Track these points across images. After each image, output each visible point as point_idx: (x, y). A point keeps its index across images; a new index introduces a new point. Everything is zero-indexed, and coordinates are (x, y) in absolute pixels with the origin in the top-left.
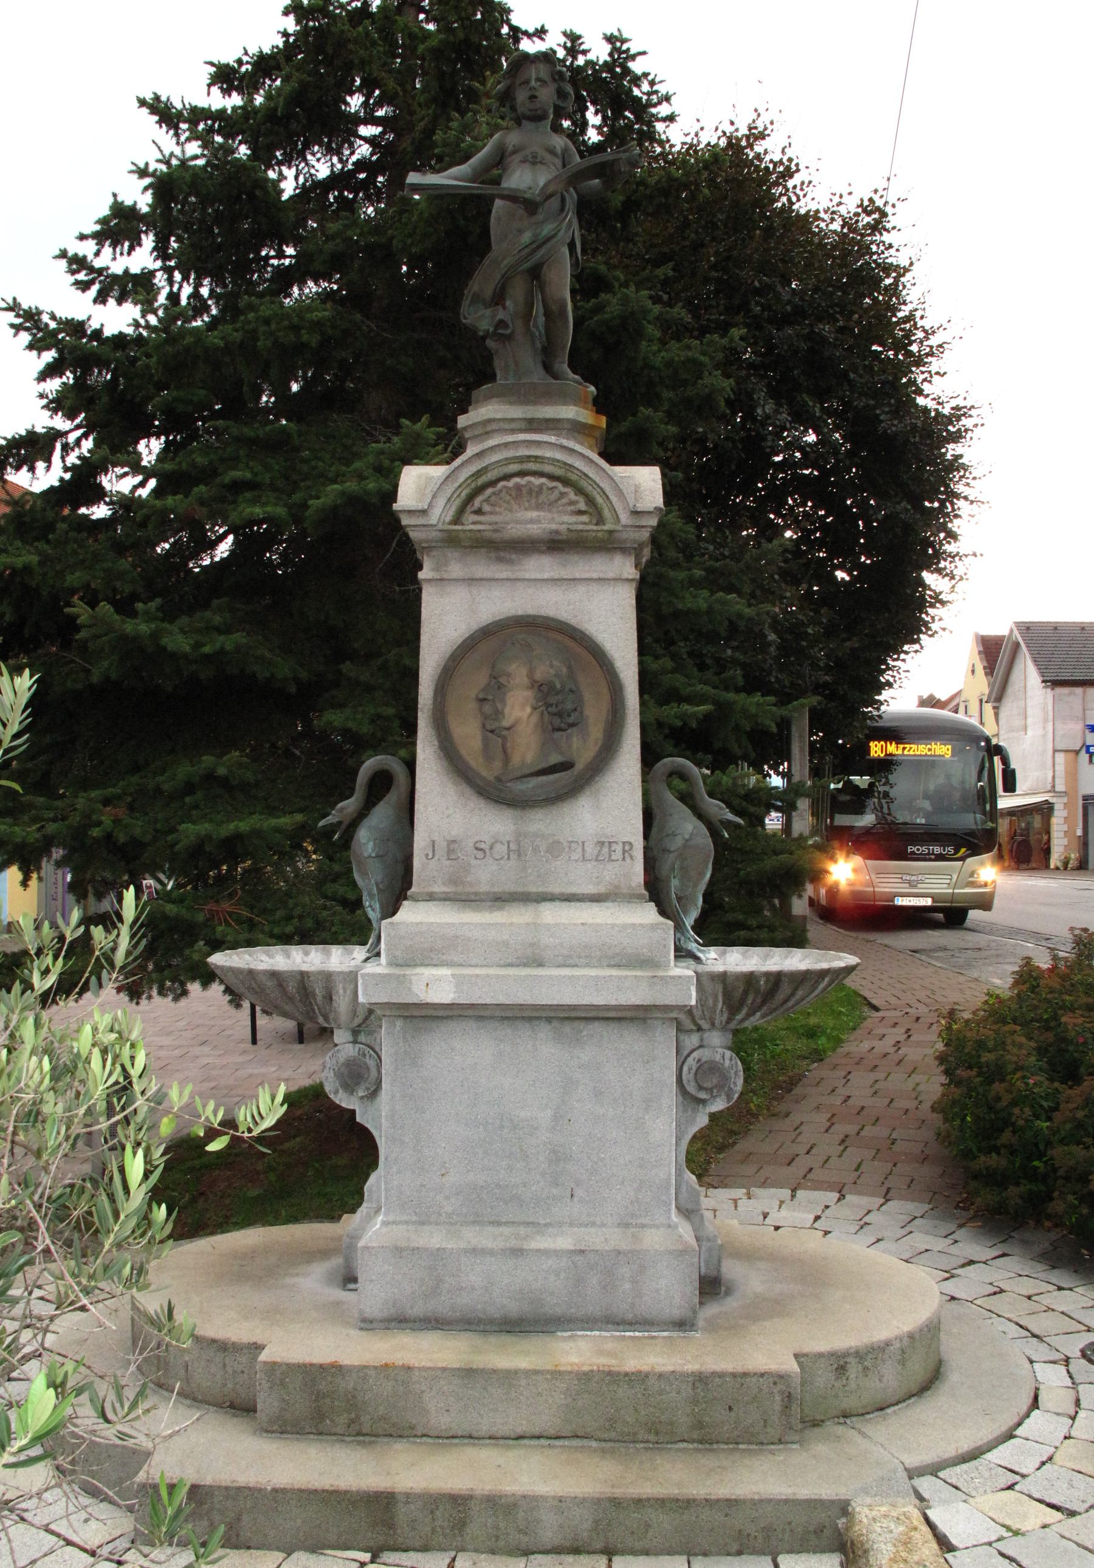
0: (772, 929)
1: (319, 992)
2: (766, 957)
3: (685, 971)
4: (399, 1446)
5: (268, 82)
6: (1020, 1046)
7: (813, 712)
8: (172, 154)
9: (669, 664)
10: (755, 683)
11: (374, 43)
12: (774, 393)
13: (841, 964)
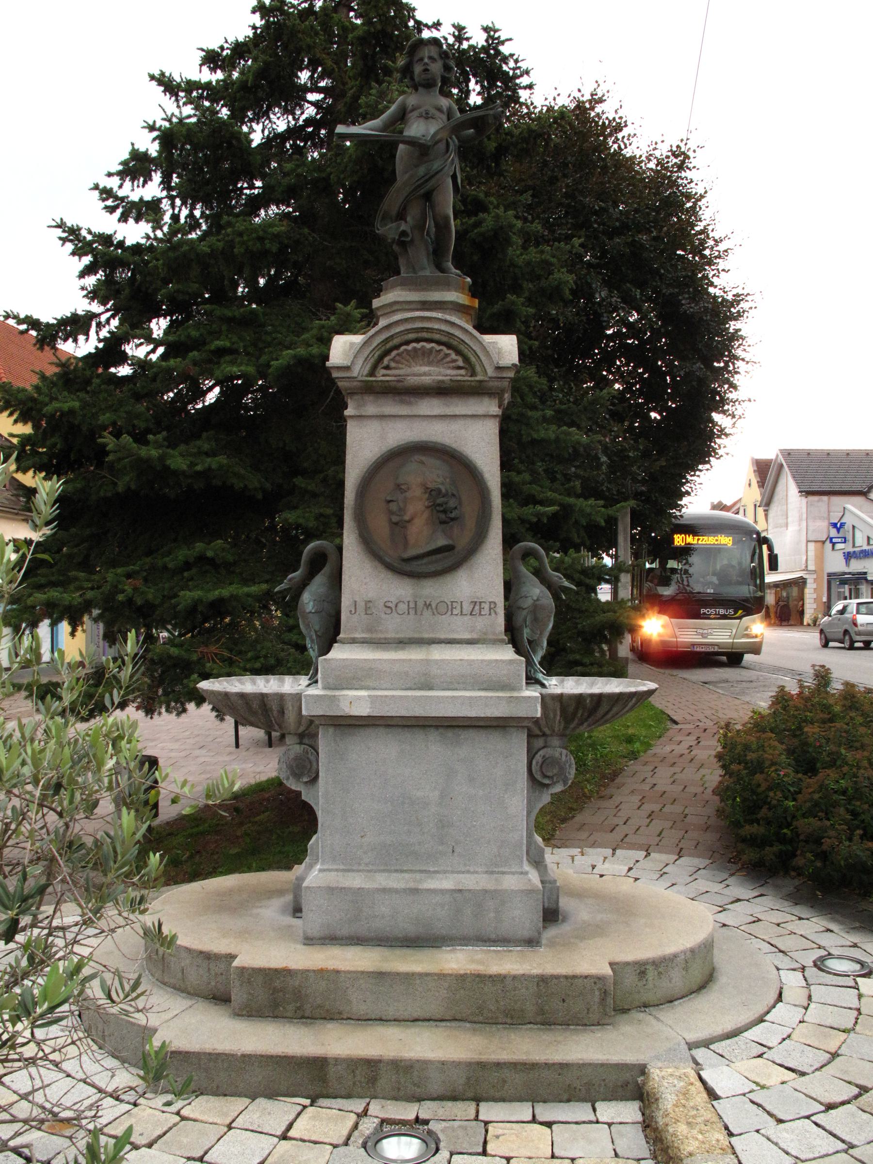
0: (600, 666)
1: (275, 708)
2: (592, 685)
3: (533, 692)
4: (330, 1025)
5: (242, 62)
6: (775, 748)
7: (634, 513)
8: (173, 114)
9: (527, 477)
10: (590, 491)
11: (317, 34)
12: (609, 284)
13: (645, 689)
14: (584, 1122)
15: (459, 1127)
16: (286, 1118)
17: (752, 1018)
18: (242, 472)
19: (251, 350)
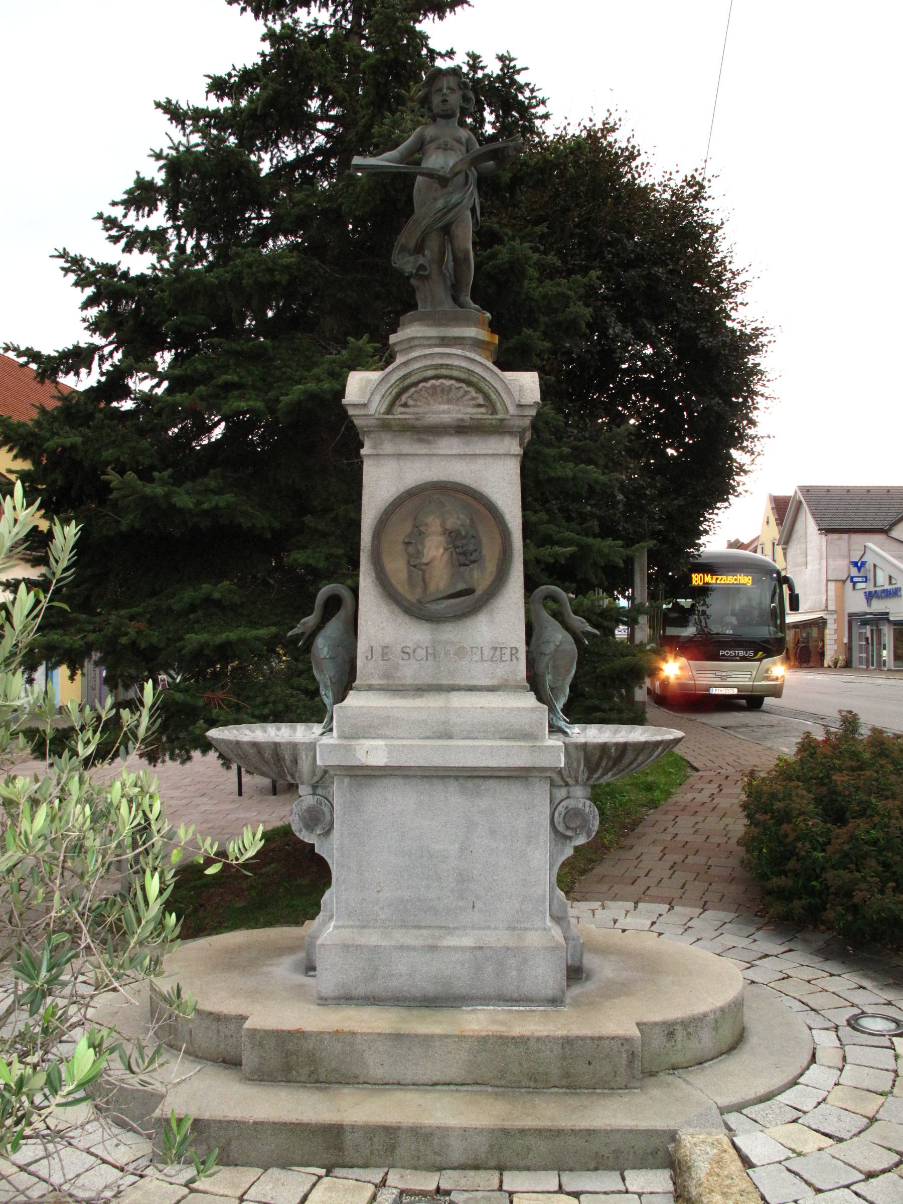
1: (288, 758)
2: (616, 732)
3: (556, 742)
4: (346, 1090)
5: (250, 90)
6: (802, 797)
7: (650, 552)
8: (180, 143)
9: (544, 516)
10: (607, 531)
11: (328, 62)
12: (622, 318)
14: (613, 1192)
15: (483, 1198)
16: (301, 1189)
17: (785, 1081)
18: (250, 510)
19: (258, 384)
